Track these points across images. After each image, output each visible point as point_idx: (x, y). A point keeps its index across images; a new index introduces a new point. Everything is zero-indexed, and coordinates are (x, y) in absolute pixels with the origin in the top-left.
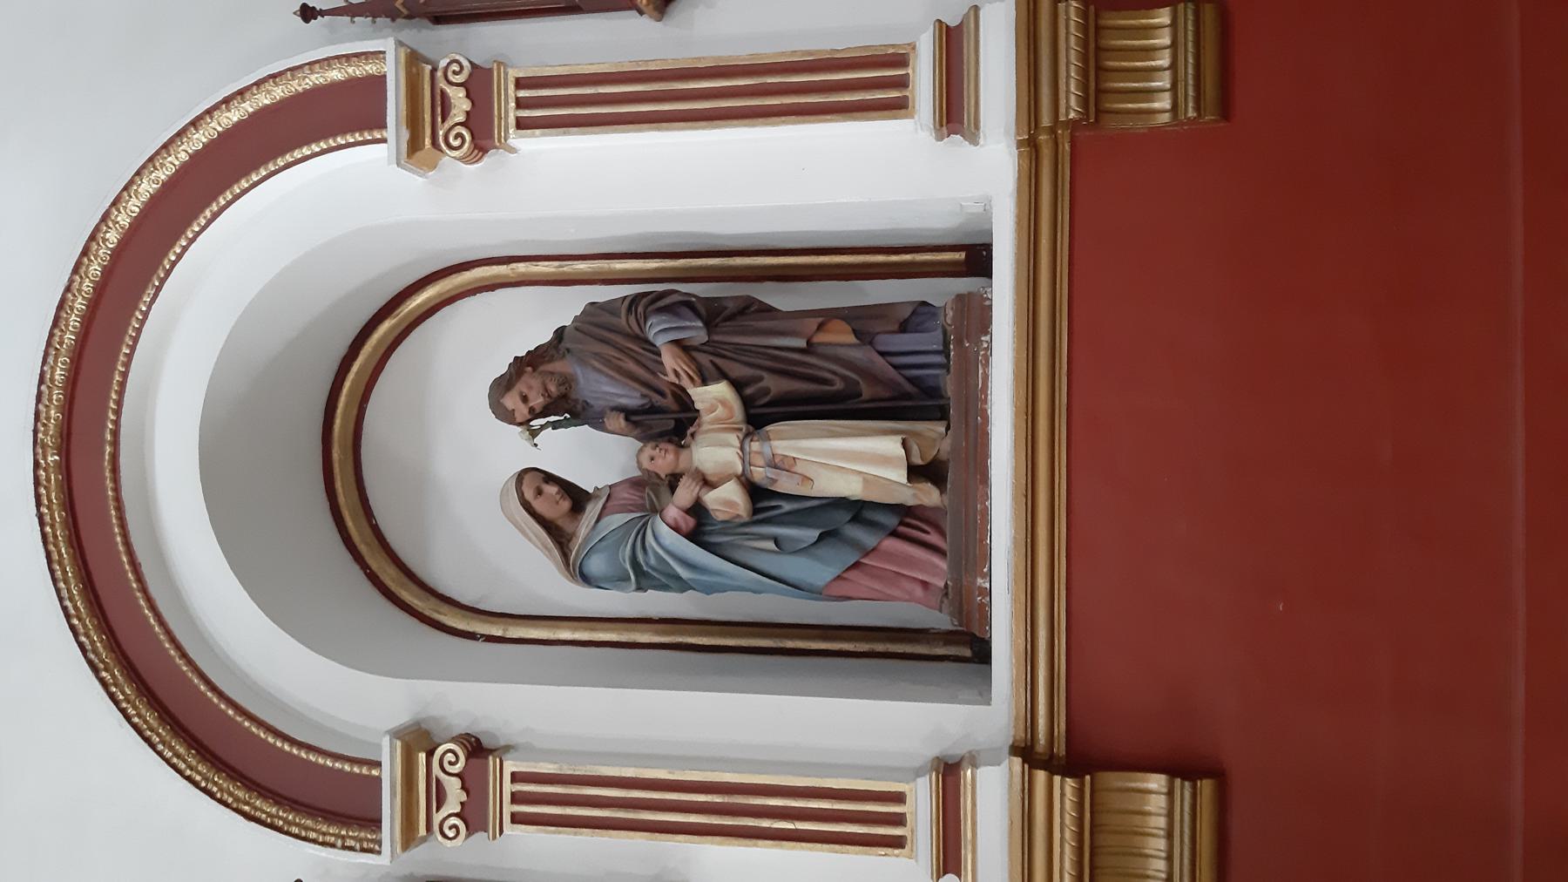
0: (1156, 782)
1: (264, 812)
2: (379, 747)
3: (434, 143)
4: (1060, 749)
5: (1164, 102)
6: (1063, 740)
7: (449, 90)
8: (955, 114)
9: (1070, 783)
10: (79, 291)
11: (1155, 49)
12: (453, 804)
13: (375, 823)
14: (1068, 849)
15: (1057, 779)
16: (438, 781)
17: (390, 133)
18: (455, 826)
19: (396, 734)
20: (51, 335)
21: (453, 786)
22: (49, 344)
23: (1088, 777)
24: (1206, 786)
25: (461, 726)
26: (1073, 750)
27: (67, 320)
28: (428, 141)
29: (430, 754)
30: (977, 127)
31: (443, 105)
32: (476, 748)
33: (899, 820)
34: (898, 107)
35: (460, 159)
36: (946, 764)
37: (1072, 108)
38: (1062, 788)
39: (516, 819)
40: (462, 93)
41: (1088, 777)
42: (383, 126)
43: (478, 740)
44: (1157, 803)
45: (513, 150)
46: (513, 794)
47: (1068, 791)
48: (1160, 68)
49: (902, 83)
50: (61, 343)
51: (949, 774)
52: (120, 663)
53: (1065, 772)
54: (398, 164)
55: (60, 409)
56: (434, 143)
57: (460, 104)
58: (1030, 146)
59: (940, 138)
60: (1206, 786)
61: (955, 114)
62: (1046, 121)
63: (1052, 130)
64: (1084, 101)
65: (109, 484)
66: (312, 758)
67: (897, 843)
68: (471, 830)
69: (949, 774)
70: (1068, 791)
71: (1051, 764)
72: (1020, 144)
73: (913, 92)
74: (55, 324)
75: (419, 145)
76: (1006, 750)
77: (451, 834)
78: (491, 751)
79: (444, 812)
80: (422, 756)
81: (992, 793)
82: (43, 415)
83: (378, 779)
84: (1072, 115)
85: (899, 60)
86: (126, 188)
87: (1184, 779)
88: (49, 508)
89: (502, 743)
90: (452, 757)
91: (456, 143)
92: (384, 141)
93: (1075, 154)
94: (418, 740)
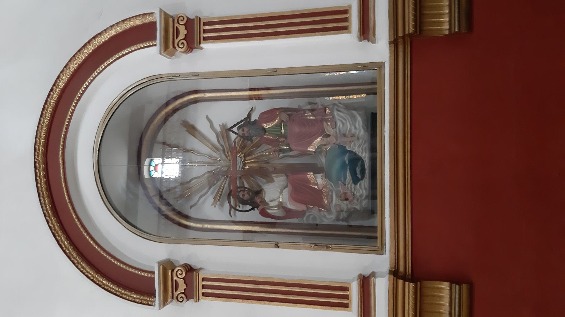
0: (445, 286)
1: (113, 289)
2: (154, 267)
3: (174, 47)
4: (409, 270)
5: (446, 26)
6: (410, 269)
7: (178, 280)
8: (366, 32)
9: (412, 285)
10: (50, 104)
11: (442, 14)
12: (182, 36)
13: (153, 295)
14: (411, 292)
15: (407, 283)
16: (176, 281)
17: (158, 41)
18: (182, 297)
19: (160, 264)
20: (40, 120)
21: (181, 282)
22: (39, 123)
23: (419, 283)
24: (465, 287)
25: (182, 263)
26: (412, 274)
27: (46, 115)
28: (171, 46)
29: (173, 271)
30: (374, 36)
31: (176, 286)
32: (189, 269)
33: (347, 297)
34: (345, 29)
35: (183, 52)
36: (364, 276)
37: (410, 29)
38: (409, 287)
39: (204, 294)
40: (184, 27)
41: (419, 283)
42: (154, 39)
43: (190, 266)
44: (446, 294)
45: (202, 49)
46: (203, 293)
47: (411, 288)
48: (444, 22)
49: (346, 20)
50: (43, 123)
51: (366, 282)
52: (64, 234)
53: (410, 281)
54: (160, 54)
55: (44, 147)
56: (174, 47)
57: (183, 31)
58: (394, 43)
59: (361, 41)
60: (465, 287)
61: (366, 32)
62: (400, 34)
63: (403, 37)
64: (415, 27)
65: (62, 143)
66: (130, 270)
67: (346, 306)
68: (188, 298)
69: (366, 282)
70: (411, 288)
71: (405, 278)
72: (390, 43)
73: (351, 15)
74: (41, 116)
75: (168, 48)
76: (388, 272)
77: (181, 300)
78: (195, 270)
79: (180, 38)
80: (170, 272)
81: (382, 289)
82: (38, 142)
83: (154, 279)
84: (411, 31)
85: (345, 12)
86: (65, 67)
87: (456, 284)
88: (39, 177)
89: (198, 267)
90: (179, 276)
91: (181, 300)
92: (155, 45)
93: (410, 42)
94: (167, 266)
